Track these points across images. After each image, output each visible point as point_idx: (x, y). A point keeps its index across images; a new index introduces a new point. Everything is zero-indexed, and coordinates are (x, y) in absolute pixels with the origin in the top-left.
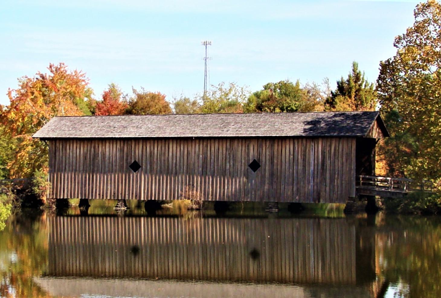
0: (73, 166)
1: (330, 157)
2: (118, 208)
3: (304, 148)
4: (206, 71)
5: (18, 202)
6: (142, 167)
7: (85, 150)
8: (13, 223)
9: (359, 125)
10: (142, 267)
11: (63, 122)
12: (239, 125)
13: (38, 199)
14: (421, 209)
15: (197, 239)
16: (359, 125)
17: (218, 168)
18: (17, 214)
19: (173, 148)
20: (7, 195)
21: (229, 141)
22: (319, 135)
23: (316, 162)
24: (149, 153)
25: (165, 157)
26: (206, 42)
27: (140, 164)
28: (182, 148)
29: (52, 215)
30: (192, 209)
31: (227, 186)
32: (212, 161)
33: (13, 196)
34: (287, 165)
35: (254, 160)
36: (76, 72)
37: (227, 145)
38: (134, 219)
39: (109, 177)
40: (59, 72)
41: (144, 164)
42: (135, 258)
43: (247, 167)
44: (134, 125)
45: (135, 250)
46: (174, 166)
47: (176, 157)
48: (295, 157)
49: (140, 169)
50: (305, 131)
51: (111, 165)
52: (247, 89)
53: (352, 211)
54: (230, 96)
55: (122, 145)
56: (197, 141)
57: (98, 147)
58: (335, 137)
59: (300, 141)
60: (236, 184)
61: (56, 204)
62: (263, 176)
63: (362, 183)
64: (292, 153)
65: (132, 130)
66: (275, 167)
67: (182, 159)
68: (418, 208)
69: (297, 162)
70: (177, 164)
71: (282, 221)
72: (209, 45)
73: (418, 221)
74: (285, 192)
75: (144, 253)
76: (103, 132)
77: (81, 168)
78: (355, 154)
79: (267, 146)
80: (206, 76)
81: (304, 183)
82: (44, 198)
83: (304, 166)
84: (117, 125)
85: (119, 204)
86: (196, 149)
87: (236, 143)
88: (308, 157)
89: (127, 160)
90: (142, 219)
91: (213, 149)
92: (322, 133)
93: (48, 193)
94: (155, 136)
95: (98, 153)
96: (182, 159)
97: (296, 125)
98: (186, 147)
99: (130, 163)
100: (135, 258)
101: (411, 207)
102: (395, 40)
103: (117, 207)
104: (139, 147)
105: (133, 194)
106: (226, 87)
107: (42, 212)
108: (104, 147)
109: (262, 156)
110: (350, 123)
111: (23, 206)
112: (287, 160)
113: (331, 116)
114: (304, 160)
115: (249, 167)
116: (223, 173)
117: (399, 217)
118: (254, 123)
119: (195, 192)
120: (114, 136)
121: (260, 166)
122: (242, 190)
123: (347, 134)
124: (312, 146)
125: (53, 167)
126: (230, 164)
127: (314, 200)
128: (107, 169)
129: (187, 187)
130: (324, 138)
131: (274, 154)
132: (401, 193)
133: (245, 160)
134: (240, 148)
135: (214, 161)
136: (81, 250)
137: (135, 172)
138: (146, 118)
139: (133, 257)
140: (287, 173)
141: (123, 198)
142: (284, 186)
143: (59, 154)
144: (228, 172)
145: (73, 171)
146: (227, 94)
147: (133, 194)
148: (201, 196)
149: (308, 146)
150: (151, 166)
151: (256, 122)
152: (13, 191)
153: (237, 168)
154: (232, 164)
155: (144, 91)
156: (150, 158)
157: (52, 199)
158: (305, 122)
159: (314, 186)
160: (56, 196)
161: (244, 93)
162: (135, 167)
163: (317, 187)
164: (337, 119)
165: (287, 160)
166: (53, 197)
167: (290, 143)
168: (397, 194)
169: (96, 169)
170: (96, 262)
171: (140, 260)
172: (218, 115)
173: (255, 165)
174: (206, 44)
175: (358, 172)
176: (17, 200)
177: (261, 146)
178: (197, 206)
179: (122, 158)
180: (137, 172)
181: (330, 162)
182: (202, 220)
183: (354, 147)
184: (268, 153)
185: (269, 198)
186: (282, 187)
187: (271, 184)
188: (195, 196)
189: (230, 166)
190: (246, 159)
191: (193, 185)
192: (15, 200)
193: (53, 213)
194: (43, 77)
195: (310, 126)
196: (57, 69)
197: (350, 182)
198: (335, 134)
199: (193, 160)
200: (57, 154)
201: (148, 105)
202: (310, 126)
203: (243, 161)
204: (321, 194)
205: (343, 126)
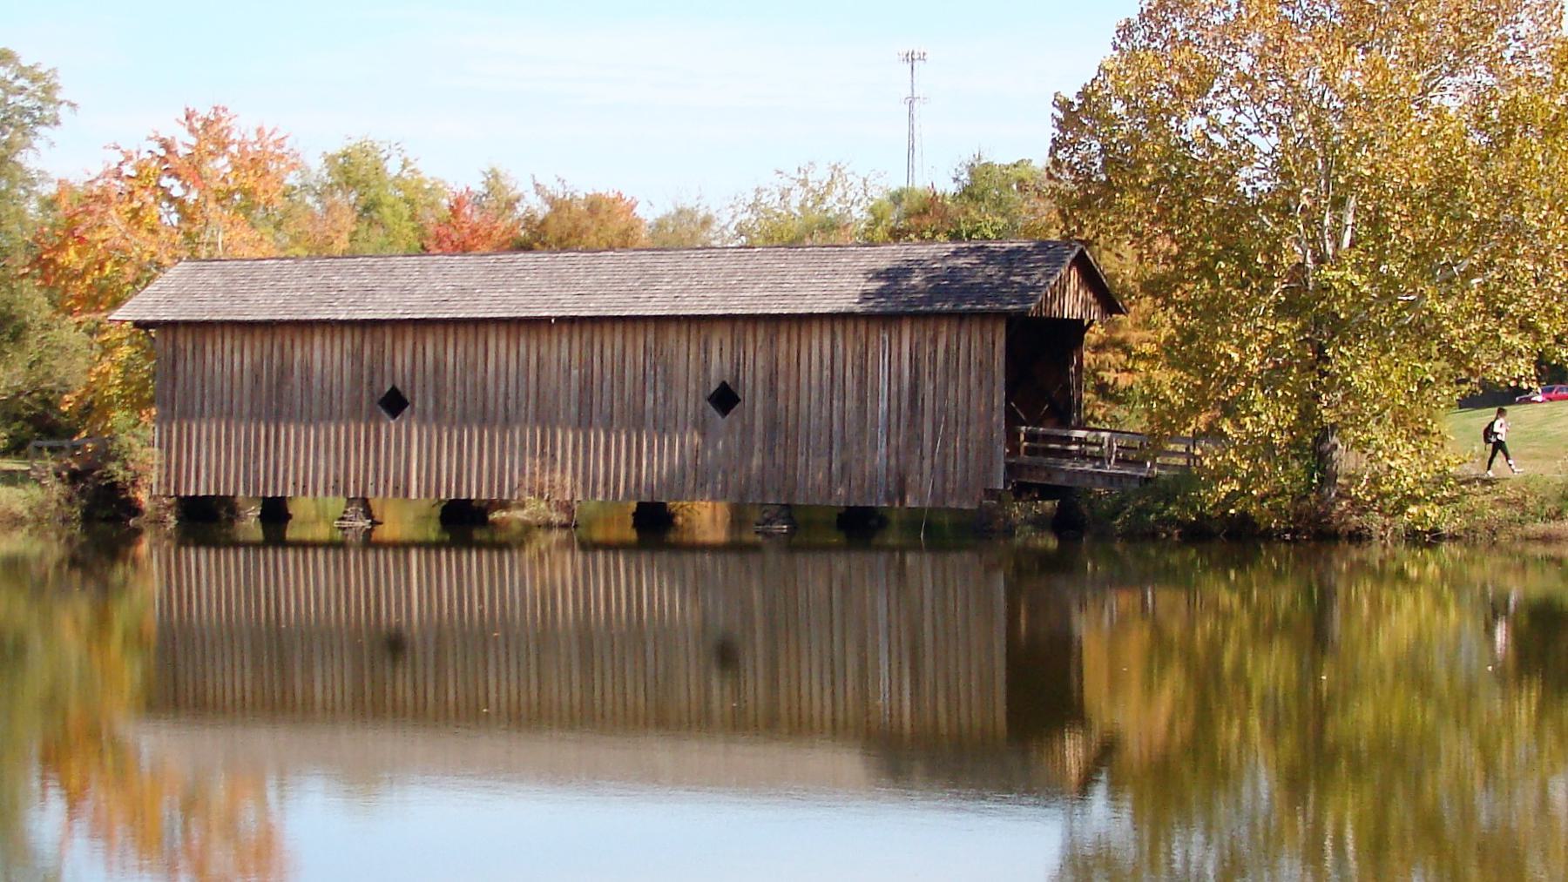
0: (222, 404)
1: (933, 374)
2: (346, 524)
3: (861, 346)
4: (911, 136)
5: (73, 507)
6: (413, 406)
7: (257, 358)
8: (59, 566)
9: (1018, 279)
10: (415, 698)
11: (201, 277)
12: (686, 281)
13: (124, 496)
14: (1180, 524)
15: (566, 610)
16: (1018, 279)
17: (622, 405)
18: (70, 540)
19: (498, 346)
20: (43, 486)
21: (653, 330)
22: (901, 308)
23: (894, 388)
24: (432, 363)
25: (476, 376)
26: (913, 53)
27: (408, 397)
28: (523, 350)
29: (166, 543)
30: (549, 526)
31: (648, 458)
32: (606, 385)
33: (58, 488)
34: (815, 395)
35: (724, 384)
36: (260, 131)
37: (648, 339)
38: (241, 553)
39: (323, 433)
40: (211, 131)
41: (418, 395)
42: (394, 666)
43: (703, 403)
44: (397, 283)
45: (395, 645)
46: (501, 400)
47: (507, 373)
48: (836, 374)
49: (408, 410)
50: (865, 297)
51: (326, 398)
52: (878, 181)
53: (992, 531)
54: (830, 200)
55: (357, 340)
56: (565, 330)
57: (292, 347)
58: (949, 315)
59: (850, 326)
60: (671, 454)
61: (176, 512)
62: (748, 430)
63: (1026, 448)
64: (827, 362)
65: (387, 298)
66: (781, 403)
67: (522, 380)
68: (1171, 520)
69: (841, 392)
70: (510, 395)
71: (800, 558)
72: (922, 62)
73: (1174, 559)
74: (807, 475)
75: (419, 656)
76: (306, 305)
77: (246, 408)
78: (1002, 366)
79: (759, 344)
80: (911, 148)
81: (861, 451)
82: (143, 496)
83: (862, 400)
84: (347, 282)
85: (349, 510)
86: (562, 350)
87: (672, 332)
88: (872, 373)
89: (371, 383)
90: (413, 554)
91: (608, 352)
92: (910, 303)
93: (154, 480)
94: (446, 316)
95: (292, 366)
96: (522, 380)
97: (844, 282)
98: (533, 345)
99: (379, 394)
100: (394, 666)
101: (1152, 517)
102: (1117, 32)
103: (343, 519)
104: (403, 347)
105: (386, 481)
106: (820, 175)
107: (138, 532)
108: (307, 349)
109: (744, 372)
110: (995, 275)
111: (88, 518)
112: (814, 382)
113: (946, 254)
114: (862, 382)
115: (708, 404)
116: (637, 422)
117: (1118, 547)
118: (727, 275)
119: (558, 476)
120: (332, 317)
121: (738, 400)
122: (689, 470)
123: (979, 307)
124: (884, 342)
125: (169, 406)
126: (655, 393)
127: (889, 498)
128: (315, 410)
129: (538, 461)
130: (915, 316)
131: (777, 365)
132: (1135, 476)
133: (697, 381)
134: (684, 348)
135: (612, 386)
136: (247, 645)
137: (394, 417)
138: (434, 262)
139: (388, 661)
140: (814, 421)
141: (360, 495)
142: (804, 457)
143: (186, 367)
144: (649, 418)
145: (224, 416)
146: (822, 199)
147: (386, 481)
148: (574, 487)
149: (873, 338)
150: (437, 402)
151: (733, 274)
152: (58, 475)
153: (673, 407)
154: (660, 394)
155: (565, 187)
156: (435, 380)
157: (164, 496)
158: (870, 272)
159: (888, 457)
160: (177, 488)
161: (869, 195)
162: (395, 403)
163: (898, 460)
164: (960, 262)
165: (814, 382)
166: (168, 491)
167: (646, 330)
168: (1124, 480)
169: (286, 410)
171: (409, 670)
172: (633, 253)
173: (725, 399)
174: (911, 58)
175: (1012, 420)
176: (69, 500)
177: (741, 341)
178: (564, 518)
179: (357, 380)
180: (398, 418)
181: (935, 388)
182: (579, 557)
183: (1001, 343)
184: (760, 363)
185: (764, 493)
186: (801, 460)
188: (558, 487)
189: (655, 400)
190: (701, 380)
191: (553, 456)
192: (62, 500)
193: (169, 537)
194: (166, 145)
195: (882, 284)
196: (207, 124)
197: (989, 440)
198: (946, 306)
199: (553, 385)
200: (180, 367)
201: (576, 227)
202: (882, 284)
203: (692, 387)
204: (909, 480)
205: (972, 284)
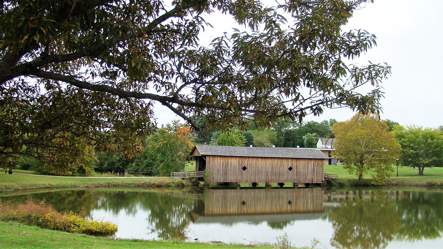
62: (294, 173)
114: (307, 167)
170: (226, 207)
173: (290, 169)
179: (239, 164)
187: (297, 175)
